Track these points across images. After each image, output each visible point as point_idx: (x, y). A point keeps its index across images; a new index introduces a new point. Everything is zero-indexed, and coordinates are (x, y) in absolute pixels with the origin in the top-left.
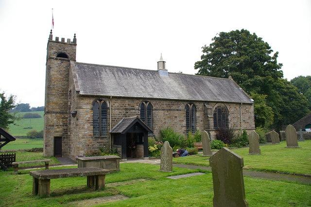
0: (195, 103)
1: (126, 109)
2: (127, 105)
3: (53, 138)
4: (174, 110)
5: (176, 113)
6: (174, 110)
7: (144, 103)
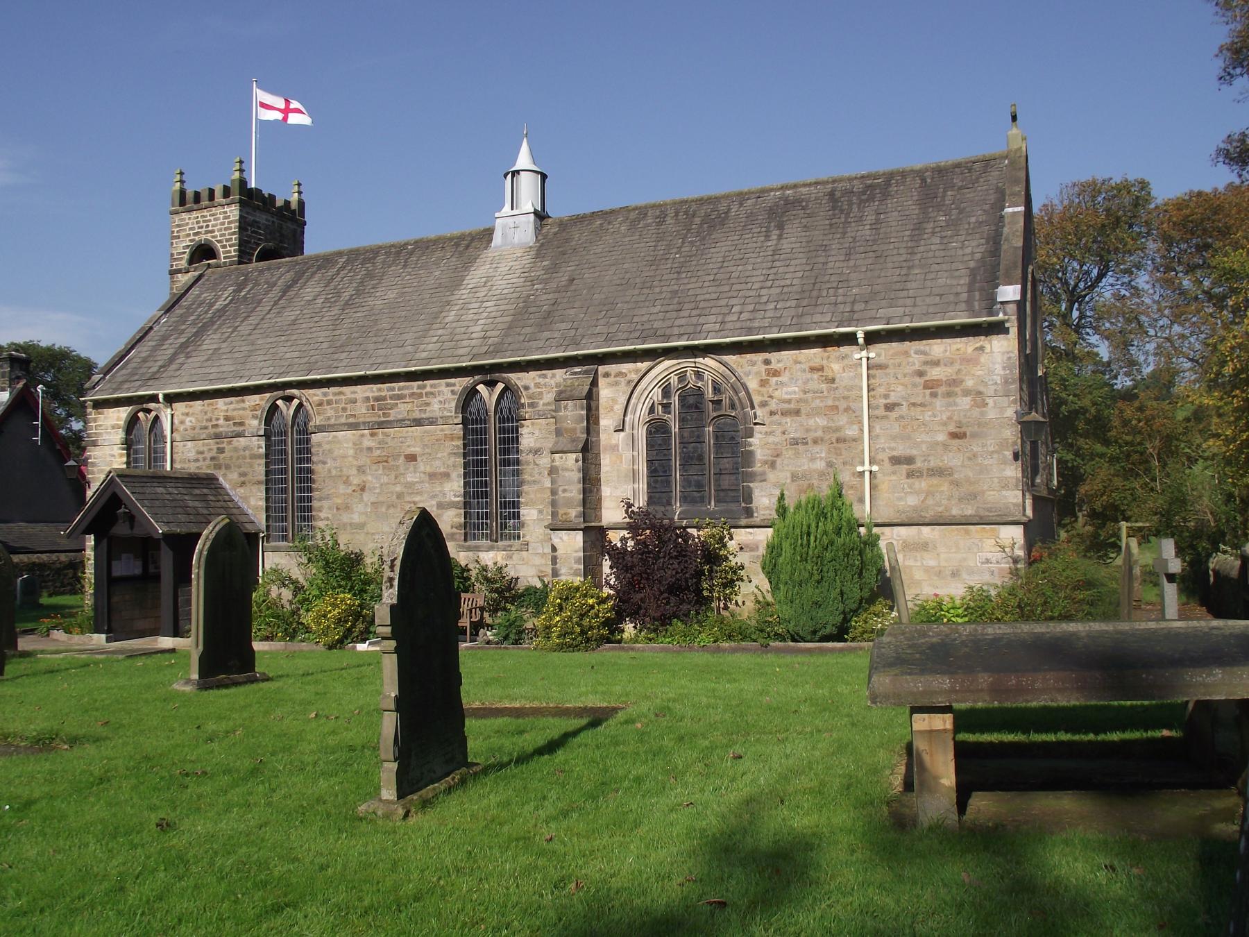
0: (514, 377)
1: (217, 436)
2: (221, 422)
3: (205, 693)
4: (401, 423)
5: (413, 439)
6: (401, 423)
7: (279, 402)
